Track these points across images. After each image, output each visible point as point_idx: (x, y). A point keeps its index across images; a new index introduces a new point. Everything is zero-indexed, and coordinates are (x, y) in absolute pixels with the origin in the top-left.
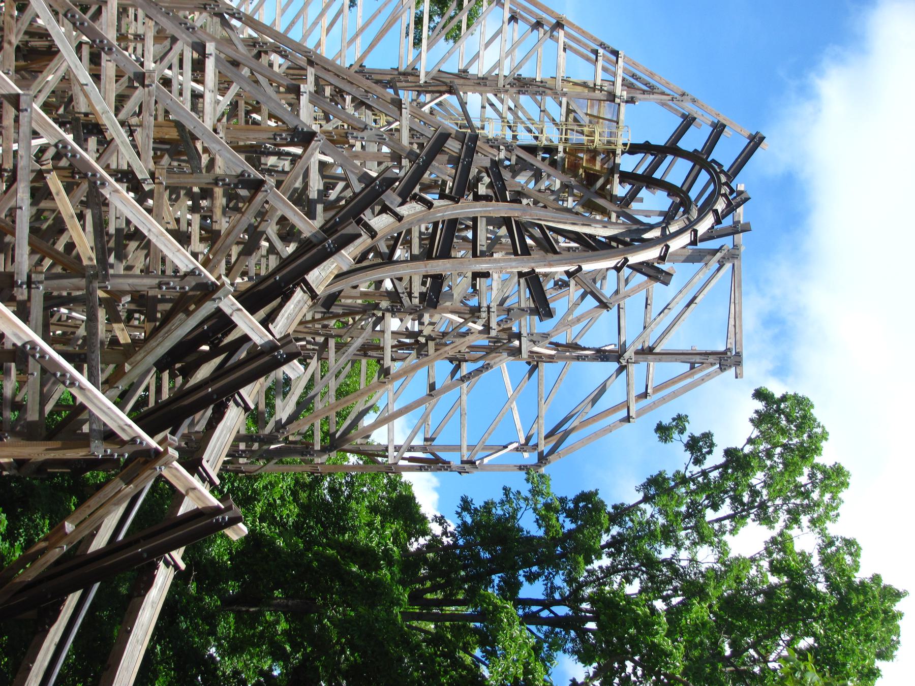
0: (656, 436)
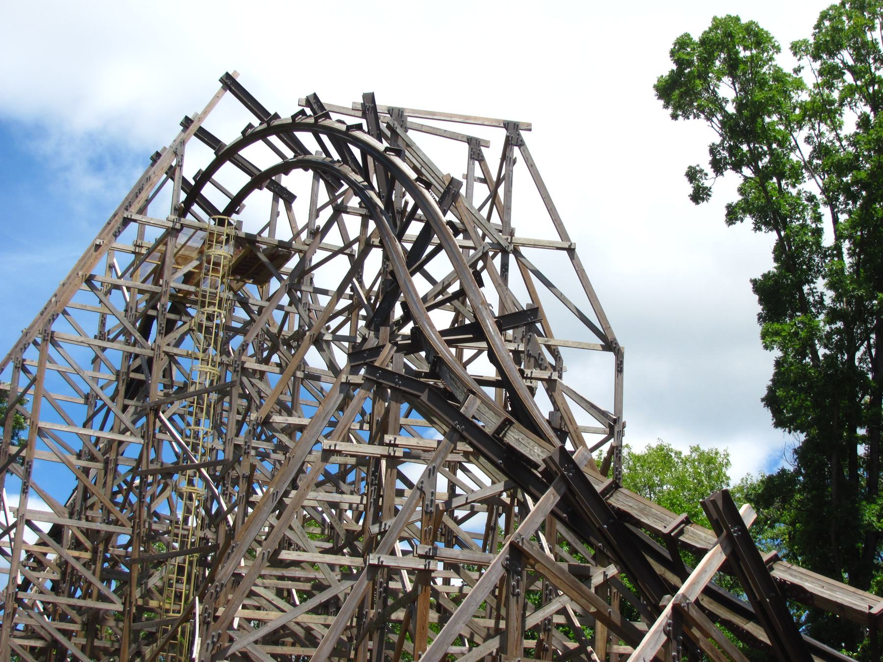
0: (703, 204)
